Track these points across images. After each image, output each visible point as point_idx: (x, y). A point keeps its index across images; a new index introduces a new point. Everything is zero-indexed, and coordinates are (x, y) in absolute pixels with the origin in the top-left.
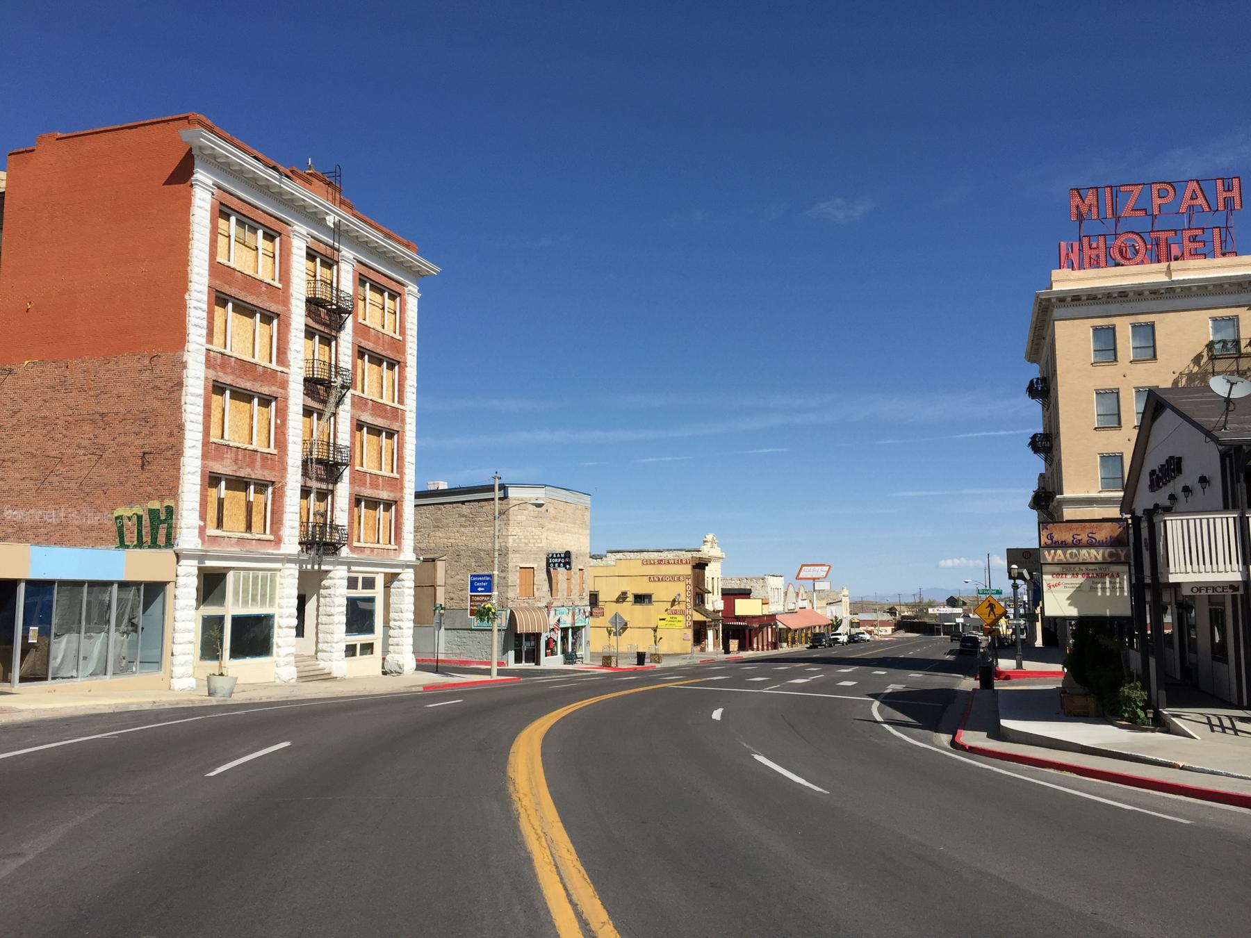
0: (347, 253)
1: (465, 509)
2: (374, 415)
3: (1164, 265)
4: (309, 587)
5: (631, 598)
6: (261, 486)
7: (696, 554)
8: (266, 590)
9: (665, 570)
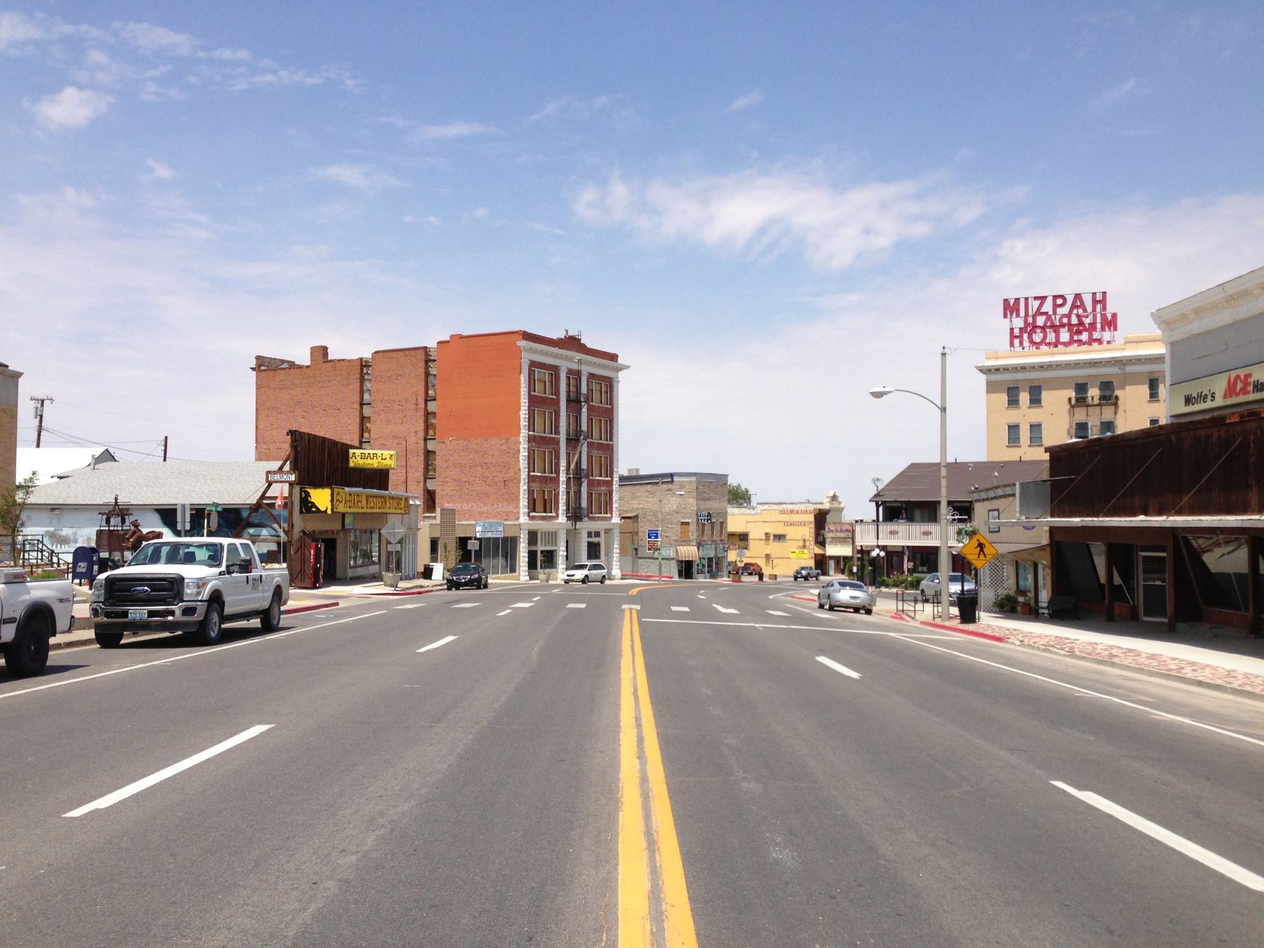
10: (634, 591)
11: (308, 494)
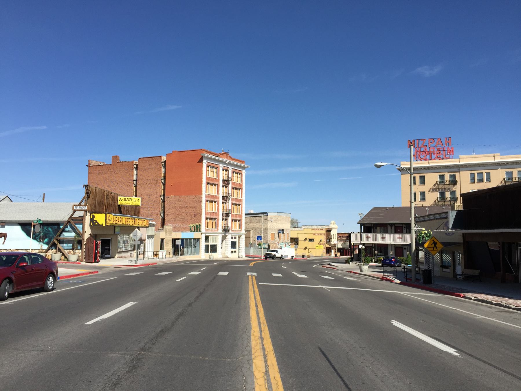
0: (230, 168)
1: (257, 218)
2: (236, 201)
3: (427, 161)
4: (224, 238)
5: (308, 240)
6: (215, 219)
7: (328, 227)
8: (215, 239)
9: (318, 232)
10: (252, 264)
11: (94, 216)
